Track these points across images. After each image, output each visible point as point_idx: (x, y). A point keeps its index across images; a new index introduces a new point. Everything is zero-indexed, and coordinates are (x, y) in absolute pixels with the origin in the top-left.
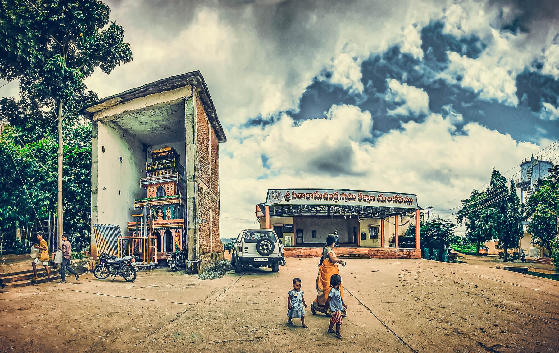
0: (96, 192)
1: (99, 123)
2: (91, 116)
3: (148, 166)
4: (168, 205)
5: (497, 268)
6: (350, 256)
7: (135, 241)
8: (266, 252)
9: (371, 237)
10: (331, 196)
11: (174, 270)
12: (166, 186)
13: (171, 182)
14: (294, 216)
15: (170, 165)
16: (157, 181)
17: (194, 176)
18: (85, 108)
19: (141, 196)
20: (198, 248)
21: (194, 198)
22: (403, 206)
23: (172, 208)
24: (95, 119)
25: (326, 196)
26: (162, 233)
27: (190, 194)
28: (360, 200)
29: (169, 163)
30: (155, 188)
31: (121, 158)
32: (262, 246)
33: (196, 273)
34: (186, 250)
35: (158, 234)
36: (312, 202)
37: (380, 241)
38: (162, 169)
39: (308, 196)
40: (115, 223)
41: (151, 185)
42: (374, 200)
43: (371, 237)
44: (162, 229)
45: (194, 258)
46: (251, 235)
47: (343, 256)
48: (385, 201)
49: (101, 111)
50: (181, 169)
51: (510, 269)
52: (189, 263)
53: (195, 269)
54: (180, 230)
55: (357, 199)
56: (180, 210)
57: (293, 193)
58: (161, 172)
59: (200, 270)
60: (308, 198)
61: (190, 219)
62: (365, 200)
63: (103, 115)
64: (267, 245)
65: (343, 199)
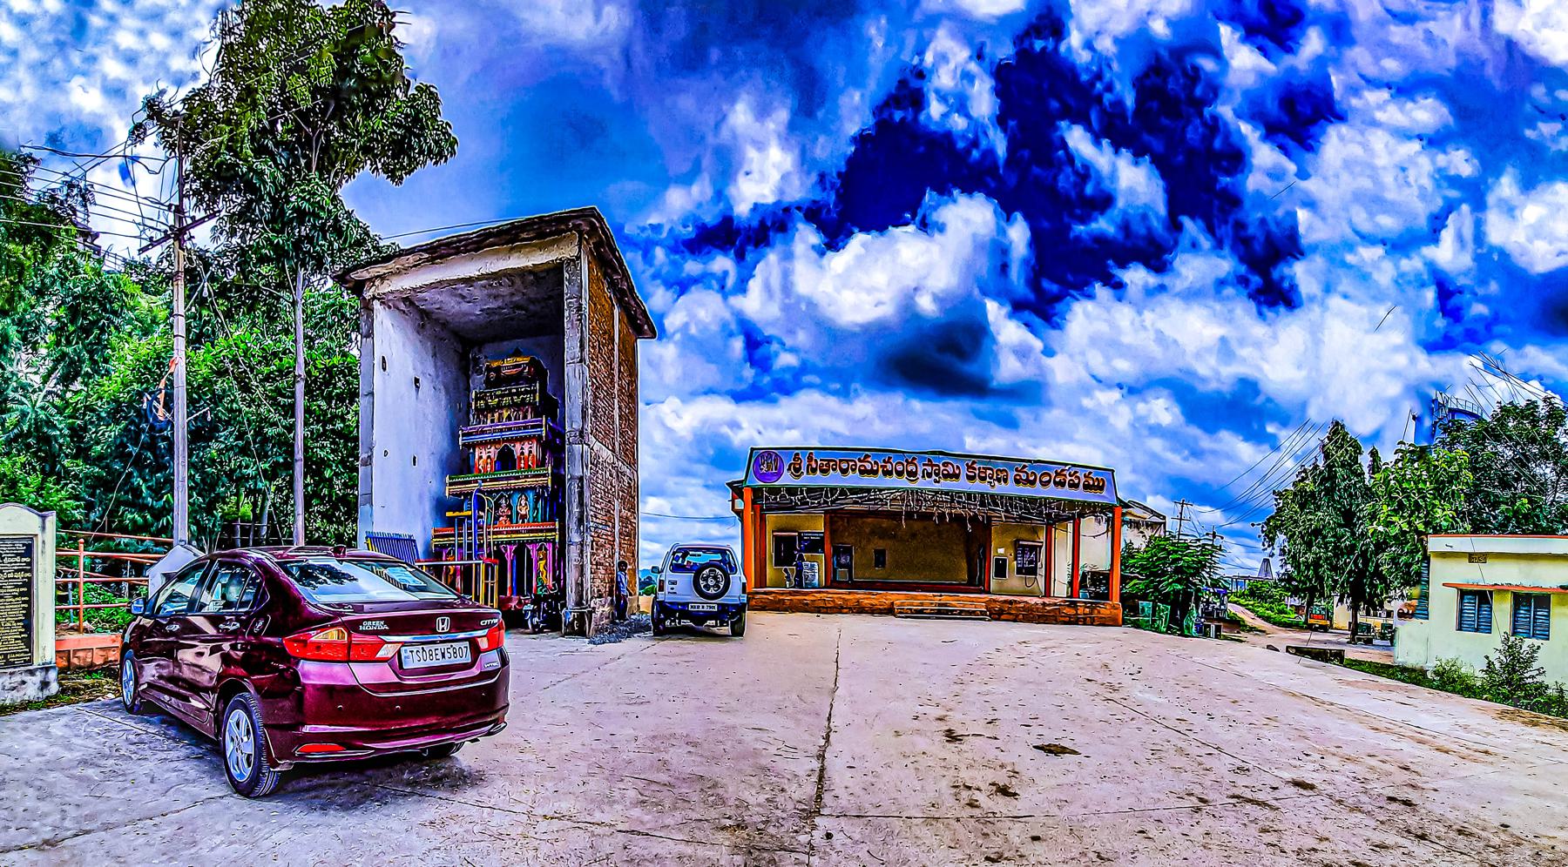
0: (368, 462)
1: (376, 304)
2: (358, 288)
3: (477, 399)
4: (523, 490)
5: (1269, 647)
6: (939, 612)
7: (448, 570)
8: (712, 591)
9: (1019, 571)
10: (900, 468)
11: (537, 630)
12: (518, 446)
13: (528, 439)
14: (826, 512)
15: (528, 398)
16: (497, 436)
17: (581, 432)
18: (347, 271)
19: (458, 463)
20: (587, 585)
21: (581, 479)
22: (1079, 495)
23: (531, 495)
24: (368, 295)
25: (889, 467)
26: (509, 555)
27: (574, 470)
28: (970, 478)
29: (526, 392)
30: (493, 451)
31: (417, 381)
32: (706, 579)
33: (581, 633)
34: (563, 590)
35: (499, 555)
36: (854, 480)
37: (1041, 581)
38: (509, 407)
39: (844, 466)
40: (404, 532)
41: (484, 444)
42: (1005, 481)
43: (1019, 571)
44: (509, 543)
45: (579, 603)
46: (684, 557)
47: (921, 611)
48: (1033, 483)
49: (382, 278)
50: (551, 407)
51: (1300, 652)
52: (569, 613)
53: (582, 625)
54: (549, 546)
55: (963, 477)
56: (554, 503)
57: (810, 458)
58: (506, 415)
59: (590, 629)
60: (844, 472)
61: (572, 524)
62: (983, 479)
63: (385, 288)
64: (715, 578)
65: (929, 475)
